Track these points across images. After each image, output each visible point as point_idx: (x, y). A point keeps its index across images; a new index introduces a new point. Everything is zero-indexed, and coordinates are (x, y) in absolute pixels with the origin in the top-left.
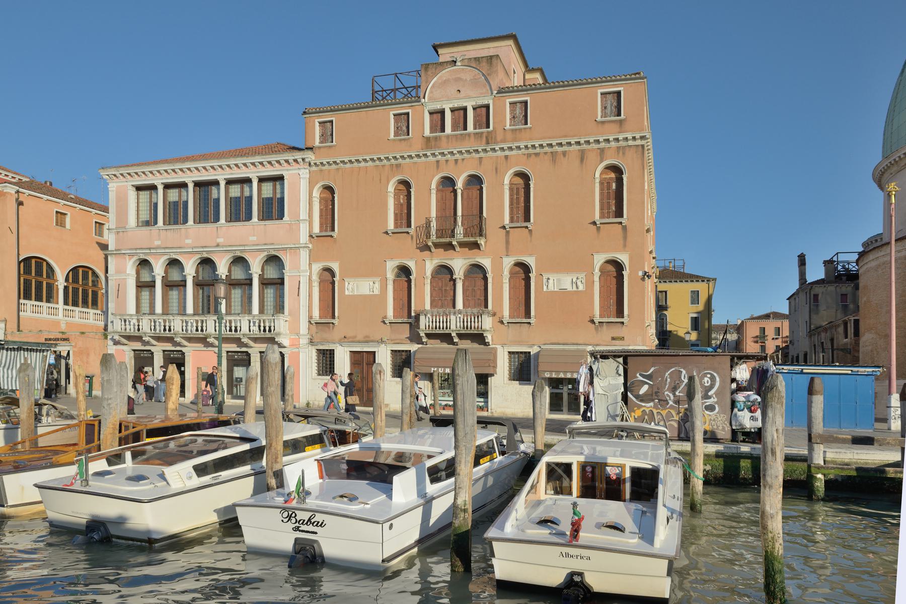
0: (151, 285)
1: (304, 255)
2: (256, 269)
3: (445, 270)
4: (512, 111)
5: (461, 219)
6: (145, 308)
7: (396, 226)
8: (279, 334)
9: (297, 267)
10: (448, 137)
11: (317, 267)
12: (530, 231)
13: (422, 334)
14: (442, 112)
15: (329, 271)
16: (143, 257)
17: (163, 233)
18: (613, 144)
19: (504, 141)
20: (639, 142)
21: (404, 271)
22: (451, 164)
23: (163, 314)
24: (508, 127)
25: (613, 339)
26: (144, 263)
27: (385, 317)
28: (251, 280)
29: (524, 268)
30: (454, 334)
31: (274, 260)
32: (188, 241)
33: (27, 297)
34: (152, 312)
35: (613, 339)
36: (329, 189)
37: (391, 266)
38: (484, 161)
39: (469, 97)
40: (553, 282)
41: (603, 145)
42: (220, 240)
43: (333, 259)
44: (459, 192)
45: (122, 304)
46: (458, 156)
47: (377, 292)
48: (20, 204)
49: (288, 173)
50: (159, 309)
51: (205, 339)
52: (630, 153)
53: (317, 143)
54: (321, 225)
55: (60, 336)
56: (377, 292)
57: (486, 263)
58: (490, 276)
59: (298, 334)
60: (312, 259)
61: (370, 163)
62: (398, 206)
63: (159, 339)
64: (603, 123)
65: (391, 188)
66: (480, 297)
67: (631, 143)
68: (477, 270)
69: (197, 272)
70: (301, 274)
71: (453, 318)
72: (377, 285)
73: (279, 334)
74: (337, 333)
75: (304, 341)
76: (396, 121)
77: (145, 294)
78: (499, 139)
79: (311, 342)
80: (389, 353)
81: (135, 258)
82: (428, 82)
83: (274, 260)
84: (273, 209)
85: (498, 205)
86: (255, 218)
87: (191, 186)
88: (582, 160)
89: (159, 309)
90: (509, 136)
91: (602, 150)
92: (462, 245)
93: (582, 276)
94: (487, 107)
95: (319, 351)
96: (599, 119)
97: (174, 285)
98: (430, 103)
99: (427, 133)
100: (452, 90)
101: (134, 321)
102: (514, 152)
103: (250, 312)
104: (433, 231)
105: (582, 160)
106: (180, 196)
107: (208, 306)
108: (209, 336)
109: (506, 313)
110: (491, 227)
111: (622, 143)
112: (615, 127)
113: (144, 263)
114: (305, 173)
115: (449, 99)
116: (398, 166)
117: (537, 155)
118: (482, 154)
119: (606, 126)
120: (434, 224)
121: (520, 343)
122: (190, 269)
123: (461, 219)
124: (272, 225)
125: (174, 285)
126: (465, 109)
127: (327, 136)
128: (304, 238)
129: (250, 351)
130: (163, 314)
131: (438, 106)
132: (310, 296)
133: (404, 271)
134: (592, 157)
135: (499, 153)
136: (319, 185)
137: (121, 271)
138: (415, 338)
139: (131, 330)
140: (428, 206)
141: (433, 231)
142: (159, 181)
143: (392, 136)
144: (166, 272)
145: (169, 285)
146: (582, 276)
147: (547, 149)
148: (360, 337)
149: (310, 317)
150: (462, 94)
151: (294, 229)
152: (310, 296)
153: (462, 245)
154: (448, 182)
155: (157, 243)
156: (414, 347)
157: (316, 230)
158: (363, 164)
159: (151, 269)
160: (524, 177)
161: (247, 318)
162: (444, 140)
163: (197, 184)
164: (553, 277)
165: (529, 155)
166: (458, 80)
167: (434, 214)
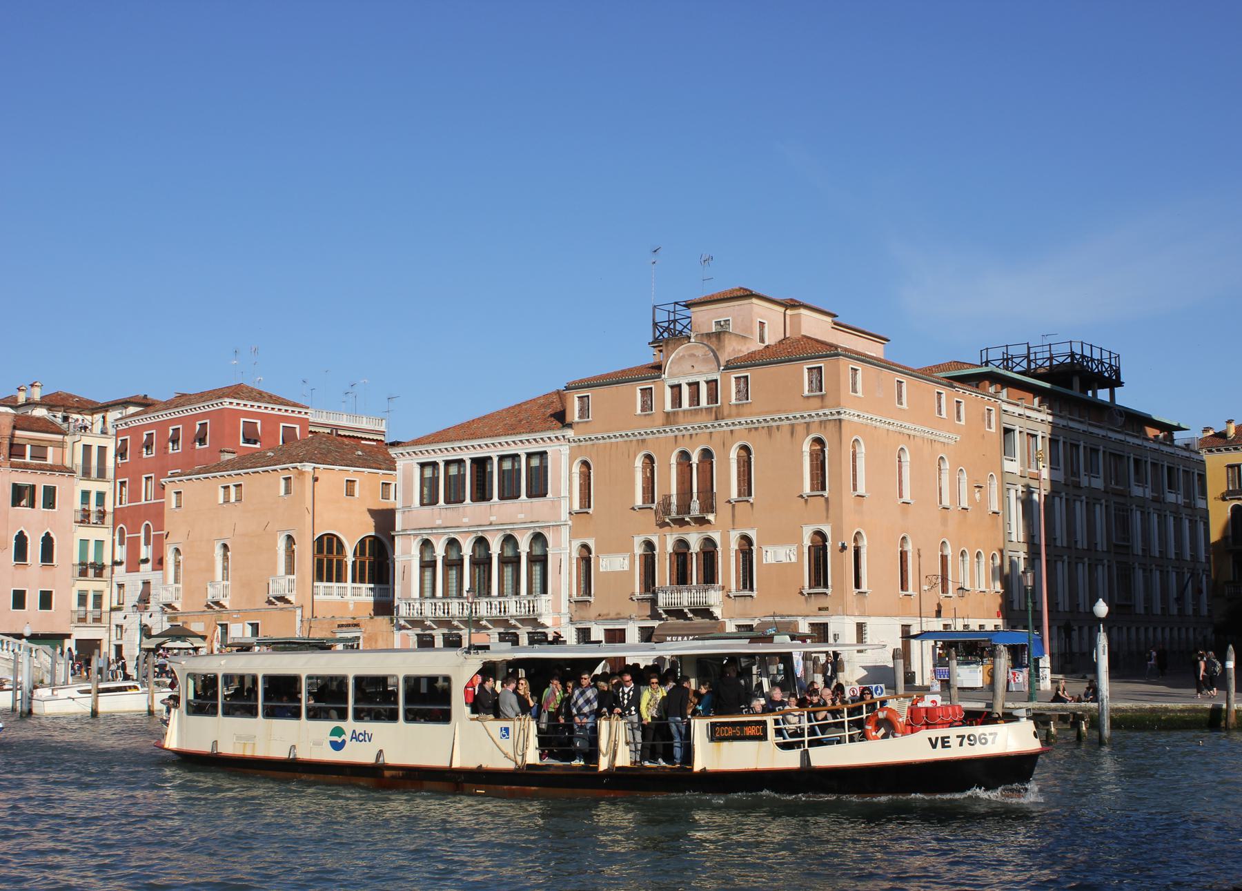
0: (433, 564)
1: (565, 532)
2: (524, 548)
3: (683, 544)
4: (738, 385)
5: (698, 478)
6: (428, 593)
7: (812, 489)
8: (540, 615)
9: (558, 544)
10: (684, 411)
11: (576, 544)
12: (827, 500)
13: (661, 611)
14: (679, 386)
15: (585, 547)
16: (425, 537)
17: (444, 512)
18: (816, 419)
19: (729, 416)
20: (836, 417)
21: (649, 545)
22: (687, 438)
23: (444, 597)
24: (733, 401)
25: (820, 609)
26: (426, 544)
27: (633, 594)
28: (435, 562)
29: (746, 539)
30: (686, 610)
31: (539, 538)
32: (466, 520)
33: (320, 579)
34: (433, 595)
35: (820, 609)
36: (586, 464)
37: (638, 541)
38: (714, 436)
39: (700, 373)
40: (770, 555)
41: (808, 420)
42: (493, 519)
43: (589, 536)
44: (694, 466)
45: (407, 587)
46: (692, 431)
47: (626, 568)
48: (316, 479)
49: (550, 449)
50: (439, 593)
51: (478, 621)
52: (830, 426)
53: (576, 419)
54: (812, 485)
55: (351, 621)
56: (626, 568)
57: (716, 536)
58: (719, 549)
59: (559, 613)
60: (573, 536)
61: (620, 439)
62: (645, 479)
63: (523, 621)
64: (808, 397)
65: (673, 460)
66: (709, 577)
67: (830, 417)
68: (709, 541)
69: (473, 550)
70: (563, 552)
71: (685, 594)
72: (627, 562)
73: (540, 615)
74: (593, 611)
75: (565, 620)
76: (643, 396)
77: (453, 573)
78: (726, 413)
79: (571, 621)
80: (637, 630)
81: (419, 538)
82: (668, 357)
83: (539, 538)
84: (538, 488)
85: (728, 483)
86: (468, 500)
87: (468, 463)
88: (792, 434)
89: (439, 593)
90: (734, 410)
91: (808, 424)
92: (675, 521)
93: (794, 548)
94: (716, 381)
95: (578, 629)
96: (806, 393)
97: (454, 564)
98: (668, 378)
99: (668, 407)
100: (686, 366)
101: (417, 606)
102: (737, 427)
103: (489, 594)
104: (674, 508)
105: (792, 434)
106: (513, 465)
107: (482, 588)
108: (480, 619)
109: (733, 587)
110: (719, 502)
111: (823, 418)
112: (817, 402)
113: (426, 544)
114: (565, 450)
115: (685, 375)
116: (643, 441)
117: (756, 429)
118: (712, 430)
119: (812, 400)
120: (674, 500)
121: (744, 616)
122: (467, 550)
123: (696, 495)
124: (537, 501)
125: (454, 564)
126: (698, 383)
127: (743, 393)
128: (565, 516)
129: (518, 632)
130: (444, 597)
131: (676, 382)
132: (570, 574)
133: (649, 545)
134: (800, 430)
135: (725, 428)
136: (811, 437)
137: (407, 552)
138: (655, 615)
139: (415, 614)
140: (670, 484)
141: (674, 508)
142: (440, 459)
143: (639, 412)
144: (446, 551)
145: (448, 564)
146: (794, 548)
147: (764, 424)
148: (612, 615)
149: (570, 596)
150: (696, 369)
151: (555, 505)
152: (570, 574)
153: (675, 521)
154: (685, 455)
155: (439, 522)
156: (656, 624)
157: (576, 507)
158: (613, 440)
159: (460, 549)
160: (745, 448)
161: (514, 599)
162: (681, 415)
163: (474, 460)
164: (771, 550)
165: (750, 430)
166: (693, 355)
167: (674, 491)
